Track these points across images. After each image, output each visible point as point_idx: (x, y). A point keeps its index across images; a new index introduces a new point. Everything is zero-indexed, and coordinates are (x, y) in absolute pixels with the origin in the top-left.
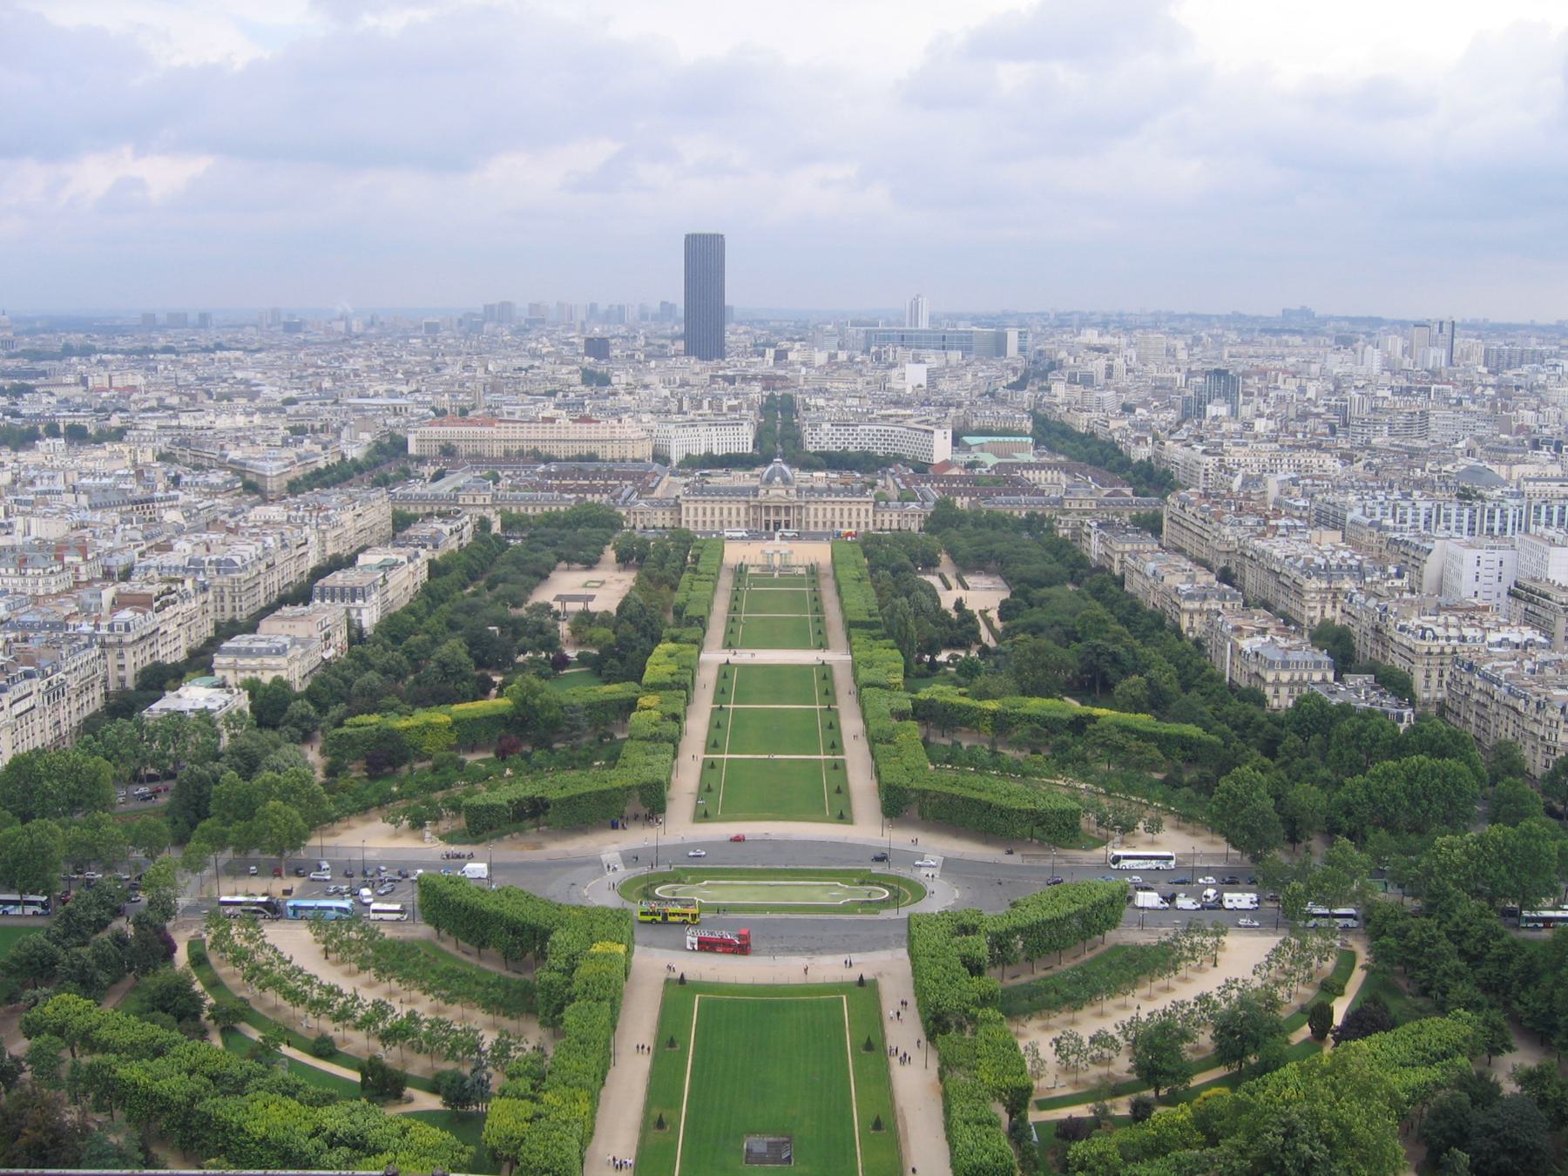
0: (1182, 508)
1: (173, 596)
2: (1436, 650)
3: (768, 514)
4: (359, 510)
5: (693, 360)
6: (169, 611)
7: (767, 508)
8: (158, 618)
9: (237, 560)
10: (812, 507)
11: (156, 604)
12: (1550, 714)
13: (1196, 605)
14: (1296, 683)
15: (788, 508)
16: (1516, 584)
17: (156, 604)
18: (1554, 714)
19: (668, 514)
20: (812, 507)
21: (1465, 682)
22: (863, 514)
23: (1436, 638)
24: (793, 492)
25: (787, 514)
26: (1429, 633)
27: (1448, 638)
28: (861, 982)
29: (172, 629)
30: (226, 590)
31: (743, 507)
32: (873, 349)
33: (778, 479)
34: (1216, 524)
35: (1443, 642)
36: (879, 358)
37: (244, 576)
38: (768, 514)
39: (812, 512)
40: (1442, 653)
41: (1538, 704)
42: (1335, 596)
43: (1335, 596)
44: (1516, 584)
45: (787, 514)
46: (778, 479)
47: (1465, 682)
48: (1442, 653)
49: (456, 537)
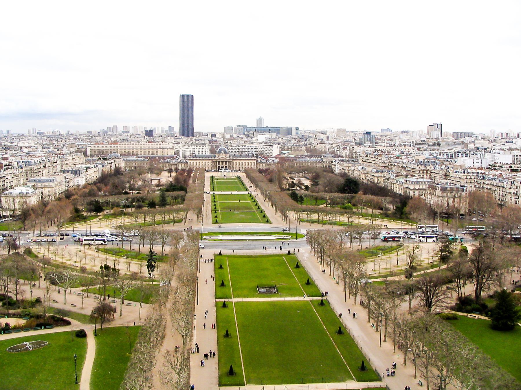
0: (367, 156)
1: (10, 167)
2: (469, 177)
3: (219, 164)
4: (74, 157)
5: (183, 137)
6: (9, 171)
7: (219, 162)
8: (6, 172)
9: (33, 161)
10: (235, 162)
11: (5, 168)
12: (516, 184)
13: (379, 175)
14: (421, 189)
15: (226, 162)
16: (489, 165)
17: (5, 168)
18: (518, 184)
19: (183, 165)
20: (235, 162)
21: (482, 183)
22: (253, 164)
23: (468, 173)
24: (228, 156)
25: (226, 164)
26: (466, 171)
27: (473, 173)
28: (289, 253)
29: (10, 178)
30: (29, 172)
31: (210, 162)
32: (246, 133)
33: (222, 152)
34: (380, 158)
35: (471, 174)
36: (248, 136)
37: (35, 167)
38: (219, 164)
39: (235, 163)
40: (471, 178)
41: (511, 182)
42: (427, 172)
43: (427, 172)
44: (489, 165)
45: (226, 164)
46: (222, 152)
47: (482, 183)
48: (471, 178)
49: (109, 166)
